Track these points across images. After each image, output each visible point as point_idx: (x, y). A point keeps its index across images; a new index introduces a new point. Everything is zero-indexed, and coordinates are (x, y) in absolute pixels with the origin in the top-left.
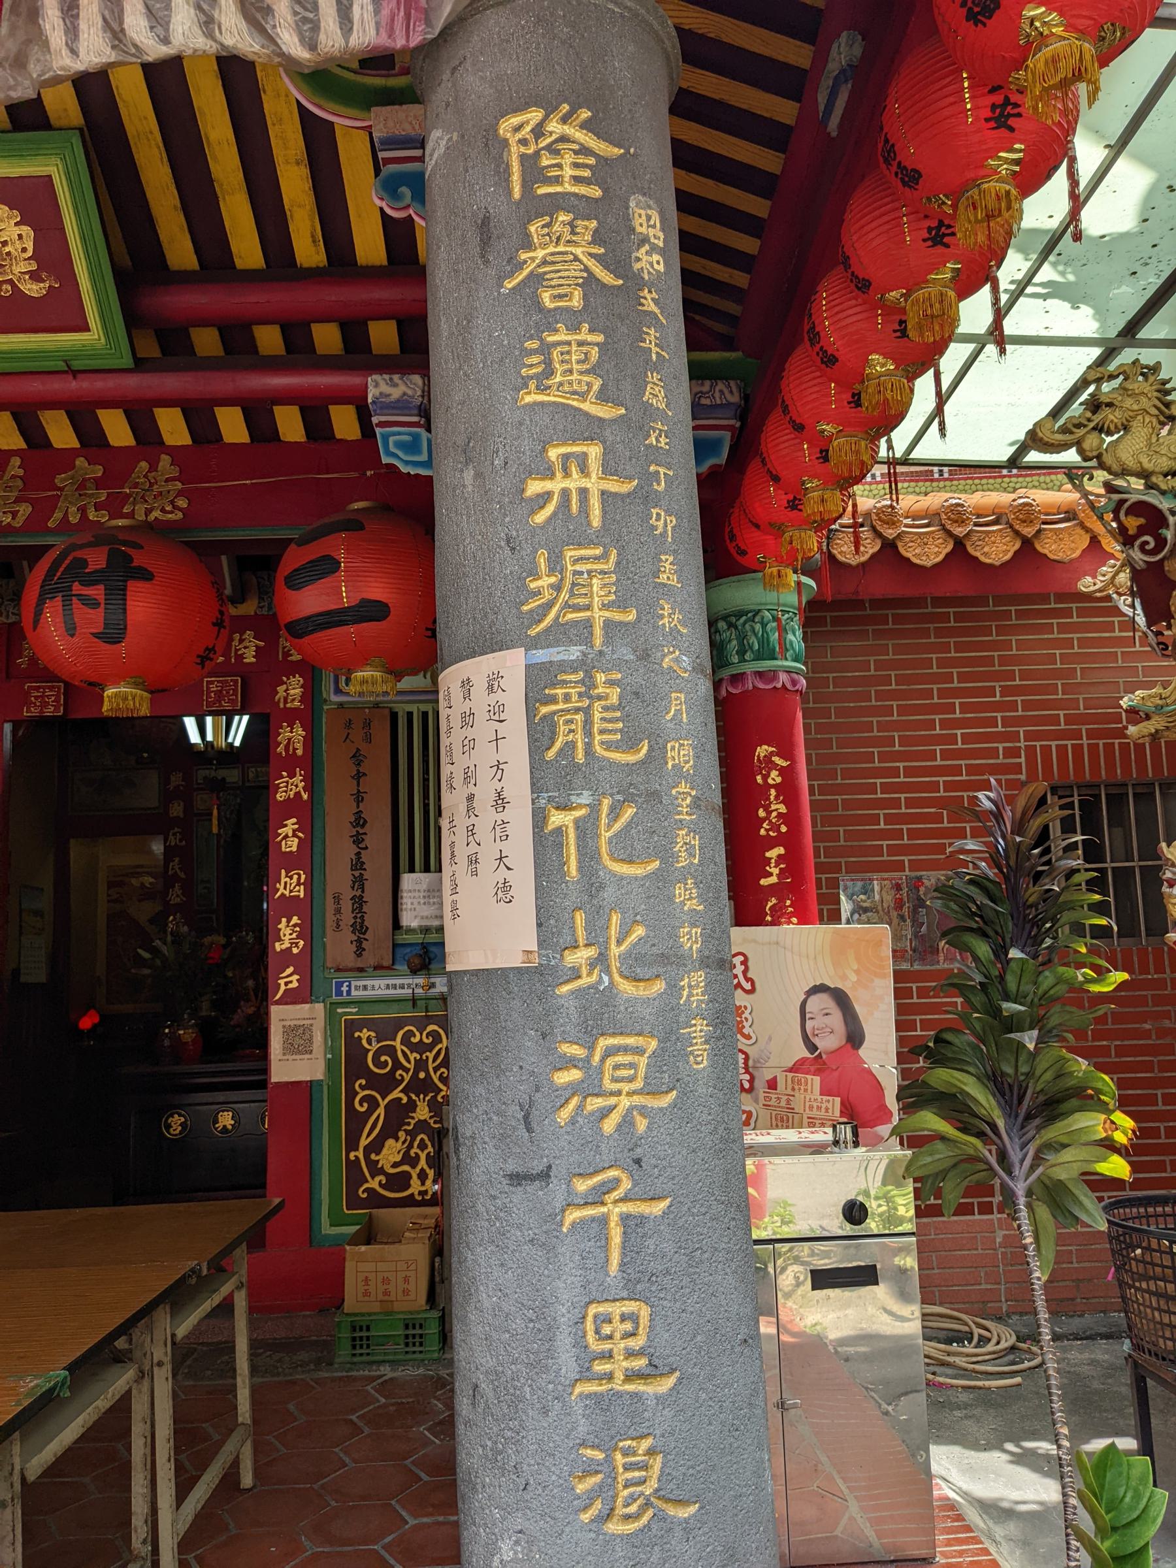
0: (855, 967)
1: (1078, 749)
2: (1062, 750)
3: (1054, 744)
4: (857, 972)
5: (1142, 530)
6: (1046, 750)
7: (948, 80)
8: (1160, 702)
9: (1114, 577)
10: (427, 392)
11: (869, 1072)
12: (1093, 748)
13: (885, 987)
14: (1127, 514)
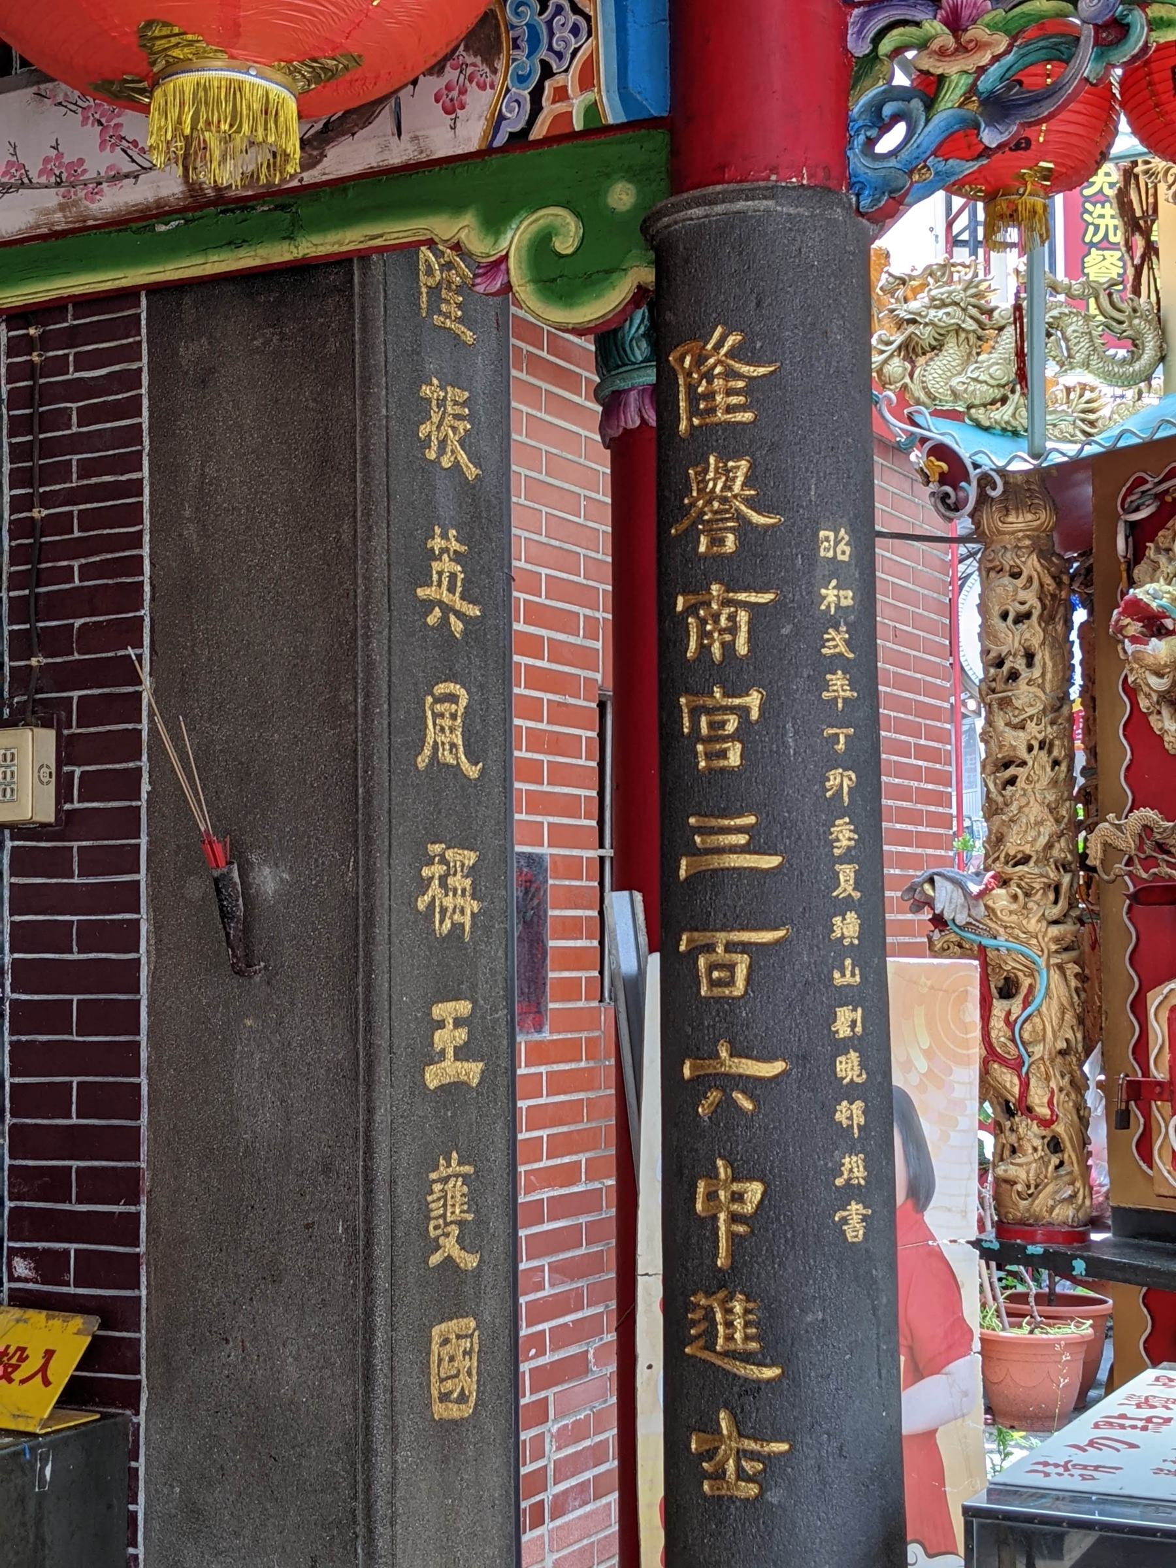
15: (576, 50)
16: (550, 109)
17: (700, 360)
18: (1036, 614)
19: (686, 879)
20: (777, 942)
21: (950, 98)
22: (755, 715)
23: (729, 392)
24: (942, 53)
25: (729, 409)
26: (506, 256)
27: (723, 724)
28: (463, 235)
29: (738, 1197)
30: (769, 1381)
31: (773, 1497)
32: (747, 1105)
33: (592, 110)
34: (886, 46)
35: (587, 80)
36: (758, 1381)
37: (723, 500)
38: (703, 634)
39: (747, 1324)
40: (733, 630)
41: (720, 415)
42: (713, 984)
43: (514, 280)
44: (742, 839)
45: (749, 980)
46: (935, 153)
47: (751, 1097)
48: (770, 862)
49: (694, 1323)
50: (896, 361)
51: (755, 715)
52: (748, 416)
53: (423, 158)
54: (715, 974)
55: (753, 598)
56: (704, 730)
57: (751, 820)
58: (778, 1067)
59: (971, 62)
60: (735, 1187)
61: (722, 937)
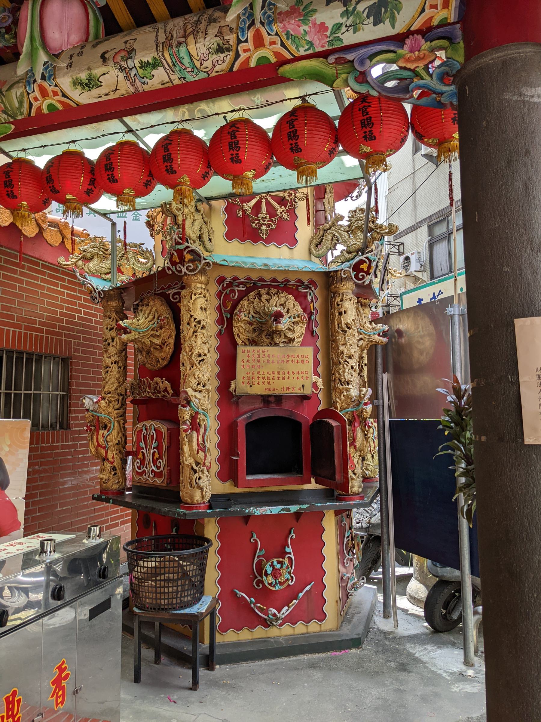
0: (9, 443)
1: (20, 333)
2: (14, 332)
3: (11, 329)
4: (9, 446)
5: (191, 261)
6: (31, 335)
7: (394, 116)
8: (138, 327)
9: (77, 261)
10: (16, 42)
11: (10, 502)
12: (26, 334)
13: (24, 454)
14: (187, 253)
18: (115, 328)
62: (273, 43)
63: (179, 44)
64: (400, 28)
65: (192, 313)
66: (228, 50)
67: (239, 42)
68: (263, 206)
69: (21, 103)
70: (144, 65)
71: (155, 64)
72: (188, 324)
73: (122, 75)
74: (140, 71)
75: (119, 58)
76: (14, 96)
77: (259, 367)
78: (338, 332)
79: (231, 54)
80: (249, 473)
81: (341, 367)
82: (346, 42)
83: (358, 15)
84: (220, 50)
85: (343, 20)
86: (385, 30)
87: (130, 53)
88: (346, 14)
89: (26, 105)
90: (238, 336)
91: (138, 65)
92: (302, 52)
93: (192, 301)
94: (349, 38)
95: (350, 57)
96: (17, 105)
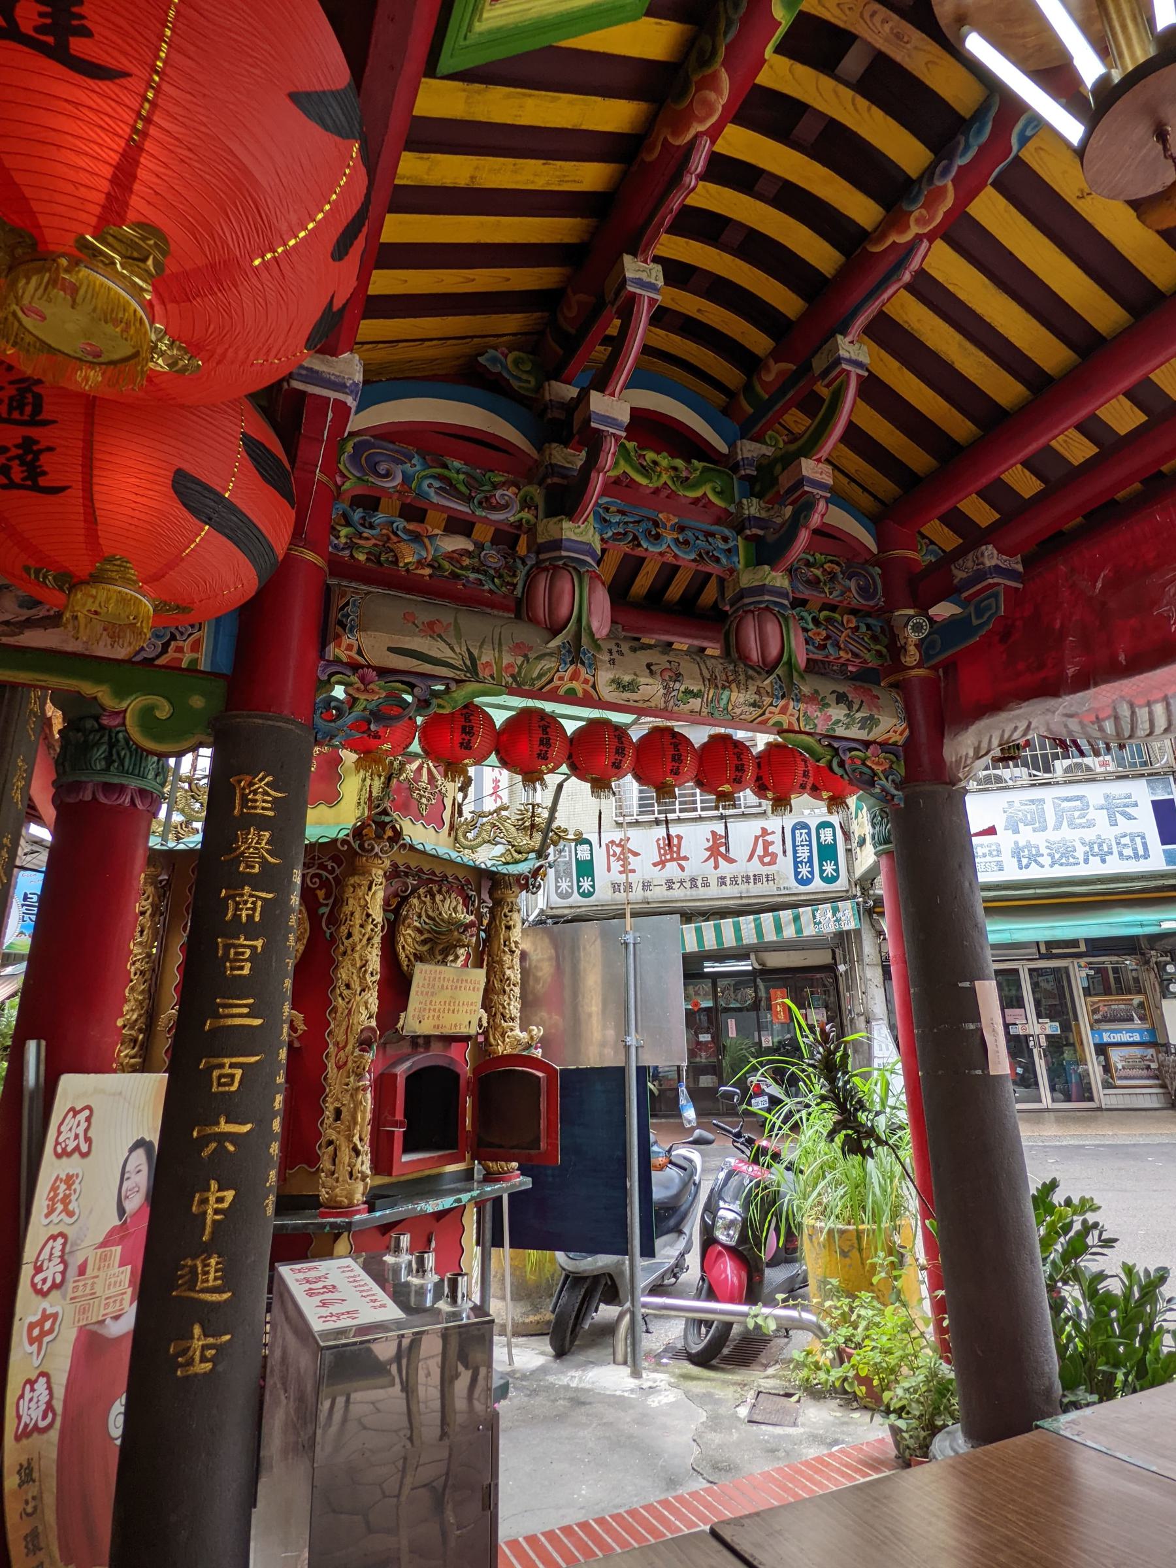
15: (190, 635)
16: (171, 653)
17: (251, 784)
18: (149, 912)
19: (209, 1030)
20: (257, 1062)
21: (359, 708)
22: (259, 950)
23: (264, 801)
24: (358, 689)
25: (263, 808)
26: (125, 711)
27: (243, 954)
28: (99, 695)
29: (220, 1200)
30: (225, 1301)
31: (220, 1368)
32: (231, 1148)
33: (195, 661)
34: (333, 679)
35: (196, 647)
36: (219, 1303)
37: (256, 849)
38: (237, 909)
39: (216, 1271)
40: (254, 909)
41: (259, 811)
42: (220, 1084)
43: (128, 722)
44: (246, 1010)
45: (241, 1083)
46: (227, 710)
47: (232, 1143)
48: (257, 1022)
49: (181, 1277)
50: (830, 839)
51: (259, 950)
52: (271, 813)
53: (87, 653)
54: (223, 1080)
55: (264, 895)
56: (232, 955)
57: (251, 1001)
58: (248, 1127)
59: (370, 697)
60: (219, 1194)
61: (227, 1061)
62: (792, 715)
63: (724, 687)
64: (871, 737)
65: (370, 912)
66: (759, 707)
67: (771, 705)
68: (425, 771)
69: (540, 676)
70: (688, 692)
71: (696, 695)
72: (362, 926)
73: (662, 691)
74: (681, 695)
75: (666, 676)
76: (540, 667)
77: (432, 994)
78: (504, 952)
79: (761, 711)
80: (406, 1150)
81: (506, 998)
82: (837, 734)
83: (854, 719)
84: (754, 705)
85: (842, 718)
86: (862, 735)
87: (678, 677)
88: (847, 716)
89: (544, 680)
90: (403, 947)
91: (682, 689)
92: (807, 729)
93: (371, 893)
94: (840, 731)
95: (836, 745)
96: (535, 675)
